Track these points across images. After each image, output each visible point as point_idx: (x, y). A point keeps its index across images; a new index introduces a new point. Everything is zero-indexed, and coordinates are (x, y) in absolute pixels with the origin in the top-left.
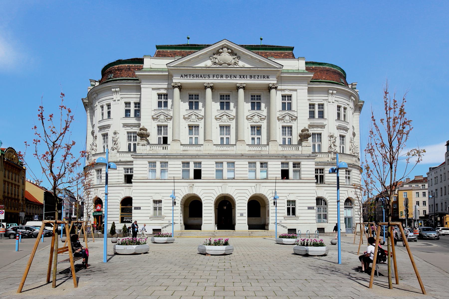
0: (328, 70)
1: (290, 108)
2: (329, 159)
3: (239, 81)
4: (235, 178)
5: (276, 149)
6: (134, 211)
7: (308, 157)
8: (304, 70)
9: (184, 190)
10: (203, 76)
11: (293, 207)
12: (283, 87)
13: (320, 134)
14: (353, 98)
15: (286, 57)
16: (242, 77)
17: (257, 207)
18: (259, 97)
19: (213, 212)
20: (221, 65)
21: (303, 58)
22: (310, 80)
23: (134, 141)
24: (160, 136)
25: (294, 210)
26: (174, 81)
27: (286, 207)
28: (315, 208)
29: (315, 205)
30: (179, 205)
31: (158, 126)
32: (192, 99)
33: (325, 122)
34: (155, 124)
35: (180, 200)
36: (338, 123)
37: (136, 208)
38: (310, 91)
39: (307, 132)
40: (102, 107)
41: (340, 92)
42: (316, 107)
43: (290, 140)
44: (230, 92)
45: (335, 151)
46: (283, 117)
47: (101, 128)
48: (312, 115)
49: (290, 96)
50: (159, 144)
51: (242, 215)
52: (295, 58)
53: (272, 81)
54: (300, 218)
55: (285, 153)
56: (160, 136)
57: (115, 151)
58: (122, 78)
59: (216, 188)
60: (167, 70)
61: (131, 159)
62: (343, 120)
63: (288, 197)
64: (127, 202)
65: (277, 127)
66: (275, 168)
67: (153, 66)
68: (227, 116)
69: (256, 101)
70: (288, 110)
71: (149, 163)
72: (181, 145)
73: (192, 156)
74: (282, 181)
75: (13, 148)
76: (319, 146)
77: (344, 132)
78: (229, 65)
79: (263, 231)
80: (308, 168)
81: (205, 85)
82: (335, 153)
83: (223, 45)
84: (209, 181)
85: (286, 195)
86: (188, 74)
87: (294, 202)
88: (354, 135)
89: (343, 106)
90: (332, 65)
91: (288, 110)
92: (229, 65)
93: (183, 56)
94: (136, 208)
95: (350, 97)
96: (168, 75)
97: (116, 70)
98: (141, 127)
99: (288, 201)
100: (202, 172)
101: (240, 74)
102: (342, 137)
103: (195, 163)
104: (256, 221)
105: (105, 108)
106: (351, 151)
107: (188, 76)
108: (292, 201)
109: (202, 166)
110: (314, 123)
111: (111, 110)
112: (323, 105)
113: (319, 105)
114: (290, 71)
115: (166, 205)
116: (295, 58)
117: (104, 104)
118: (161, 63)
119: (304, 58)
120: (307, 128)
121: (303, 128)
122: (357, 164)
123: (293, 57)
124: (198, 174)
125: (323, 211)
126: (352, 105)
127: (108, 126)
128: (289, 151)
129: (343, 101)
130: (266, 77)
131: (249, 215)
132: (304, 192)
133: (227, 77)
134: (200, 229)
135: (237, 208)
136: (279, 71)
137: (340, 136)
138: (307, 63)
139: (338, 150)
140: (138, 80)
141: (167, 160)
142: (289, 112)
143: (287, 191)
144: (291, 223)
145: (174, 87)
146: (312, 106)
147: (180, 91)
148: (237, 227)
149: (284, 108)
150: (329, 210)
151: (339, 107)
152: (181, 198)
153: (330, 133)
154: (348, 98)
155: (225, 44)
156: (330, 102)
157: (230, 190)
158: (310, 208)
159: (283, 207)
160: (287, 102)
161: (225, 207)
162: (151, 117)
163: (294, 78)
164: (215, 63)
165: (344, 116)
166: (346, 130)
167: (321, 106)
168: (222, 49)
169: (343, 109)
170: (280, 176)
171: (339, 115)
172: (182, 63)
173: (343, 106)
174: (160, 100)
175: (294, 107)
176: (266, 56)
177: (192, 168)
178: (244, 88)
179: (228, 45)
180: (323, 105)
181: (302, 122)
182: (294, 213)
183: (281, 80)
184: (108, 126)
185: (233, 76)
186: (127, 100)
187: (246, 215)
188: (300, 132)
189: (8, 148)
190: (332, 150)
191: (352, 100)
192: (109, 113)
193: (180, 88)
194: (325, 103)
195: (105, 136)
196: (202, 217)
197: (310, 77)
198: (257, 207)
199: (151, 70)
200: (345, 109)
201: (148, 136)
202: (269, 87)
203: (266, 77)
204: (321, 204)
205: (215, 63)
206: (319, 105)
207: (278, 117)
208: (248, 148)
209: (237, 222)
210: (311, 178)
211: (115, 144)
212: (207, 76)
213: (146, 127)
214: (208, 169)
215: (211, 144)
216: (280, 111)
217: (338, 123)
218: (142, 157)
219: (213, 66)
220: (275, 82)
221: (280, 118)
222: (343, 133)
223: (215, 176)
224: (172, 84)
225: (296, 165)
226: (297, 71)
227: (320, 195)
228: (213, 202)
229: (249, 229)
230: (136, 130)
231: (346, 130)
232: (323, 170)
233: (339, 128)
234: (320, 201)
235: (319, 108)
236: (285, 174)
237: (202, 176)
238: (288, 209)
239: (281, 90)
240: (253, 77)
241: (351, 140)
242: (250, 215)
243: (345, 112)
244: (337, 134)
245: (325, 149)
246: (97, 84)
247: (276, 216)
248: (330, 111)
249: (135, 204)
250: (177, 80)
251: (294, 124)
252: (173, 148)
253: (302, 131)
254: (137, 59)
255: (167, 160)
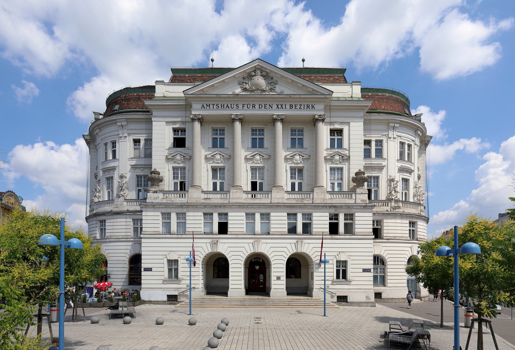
0: (388, 98)
1: (340, 146)
2: (388, 208)
3: (276, 112)
4: (271, 233)
5: (323, 197)
6: (143, 273)
7: (365, 208)
8: (359, 98)
9: (204, 249)
10: (230, 106)
11: (344, 268)
12: (333, 119)
13: (377, 178)
14: (419, 132)
15: (335, 82)
16: (280, 106)
17: (297, 266)
18: (301, 131)
19: (243, 270)
20: (253, 91)
21: (358, 82)
22: (367, 110)
23: (144, 186)
24: (176, 181)
25: (345, 272)
26: (194, 113)
27: (335, 268)
28: (372, 270)
29: (371, 267)
30: (201, 266)
31: (174, 168)
32: (256, 134)
33: (384, 163)
34: (171, 166)
35: (201, 260)
36: (400, 164)
37: (146, 270)
38: (367, 123)
39: (363, 175)
40: (106, 144)
41: (403, 124)
42: (373, 144)
43: (340, 185)
44: (264, 126)
45: (396, 199)
46: (332, 157)
47: (105, 170)
48: (367, 154)
49: (340, 132)
50: (175, 190)
51: (278, 278)
52: (347, 82)
53: (318, 111)
54: (353, 283)
55: (334, 201)
56: (176, 181)
57: (122, 199)
58: (128, 110)
59: (246, 246)
60: (184, 99)
61: (138, 208)
62: (406, 159)
63: (337, 257)
64: (135, 261)
65: (324, 169)
66: (321, 222)
67: (168, 95)
68: (260, 155)
69: (258, 137)
70: (338, 148)
71: (163, 214)
72: (203, 192)
73: (216, 206)
74: (330, 237)
75: (12, 192)
76: (376, 192)
77: (408, 175)
78: (264, 91)
79: (306, 298)
80: (364, 222)
81: (233, 116)
82: (397, 201)
83: (255, 67)
84: (238, 236)
85: (336, 254)
86: (211, 103)
87: (345, 262)
88: (419, 177)
89: (407, 142)
90: (393, 92)
91: (338, 148)
92: (264, 91)
93: (205, 81)
94: (146, 270)
95: (416, 132)
96: (186, 105)
97: (122, 100)
98: (153, 169)
99: (337, 261)
100: (229, 226)
101: (278, 103)
102: (406, 181)
103: (220, 214)
104: (296, 282)
105: (110, 146)
106: (416, 199)
107: (211, 106)
108: (343, 261)
109: (229, 218)
110: (372, 164)
111: (117, 149)
112: (381, 141)
113: (377, 141)
114: (340, 99)
115: (183, 269)
116: (347, 82)
117: (109, 141)
118: (178, 91)
119: (359, 82)
120: (362, 170)
121: (357, 171)
122: (423, 214)
123: (345, 81)
124: (223, 228)
125: (380, 272)
126: (417, 141)
127: (381, 168)
128: (338, 200)
129: (408, 137)
130: (311, 107)
131: (288, 276)
132: (357, 251)
133: (261, 107)
134: (225, 294)
135: (273, 270)
136: (327, 98)
137: (403, 179)
138: (363, 90)
139: (399, 196)
140: (148, 112)
141: (184, 211)
142: (340, 151)
143: (337, 248)
144: (341, 289)
145: (193, 120)
146: (367, 143)
147: (201, 125)
148: (271, 293)
149: (332, 146)
150: (389, 270)
151: (402, 144)
152: (203, 257)
153: (390, 176)
154: (414, 133)
155: (258, 65)
156: (391, 138)
157: (265, 247)
158: (365, 270)
159: (331, 269)
160: (218, 137)
161: (257, 270)
162: (164, 158)
163: (348, 107)
164: (245, 90)
165: (408, 154)
166: (410, 172)
167: (379, 143)
168: (255, 71)
169: (406, 146)
170: (328, 230)
171: (402, 154)
172: (202, 90)
173: (407, 142)
174: (332, 137)
175: (345, 145)
176: (311, 81)
177: (216, 220)
178: (282, 120)
179: (262, 67)
180: (381, 141)
181: (357, 163)
182: (345, 277)
183: (329, 108)
184: (113, 169)
185: (268, 106)
186: (136, 137)
187: (284, 278)
188: (353, 175)
189: (7, 192)
190: (393, 197)
191: (419, 135)
192: (114, 152)
193: (201, 120)
194: (385, 139)
195: (110, 179)
196: (228, 277)
197: (367, 106)
198: (297, 266)
199: (165, 98)
200: (409, 146)
201: (161, 181)
202: (314, 119)
203: (311, 107)
204: (378, 264)
205: (245, 90)
206: (377, 141)
207: (325, 157)
208: (286, 196)
209: (273, 287)
210: (367, 234)
211: (121, 190)
212: (235, 106)
213: (158, 170)
214: (237, 221)
215: (240, 191)
216: (327, 149)
217: (400, 164)
218: (154, 206)
219: (242, 93)
220: (322, 113)
221: (328, 157)
222: (406, 176)
223: (244, 230)
224: (191, 116)
225: (350, 217)
226: (350, 99)
227: (377, 253)
228: (243, 263)
229: (288, 294)
230: (146, 172)
231: (410, 172)
232: (380, 221)
233: (402, 170)
234: (379, 260)
235: (376, 145)
236: (334, 229)
237: (229, 230)
238: (338, 272)
239: (331, 123)
240: (294, 107)
241: (416, 184)
242: (289, 274)
243: (409, 150)
244: (398, 177)
245: (383, 195)
246: (101, 117)
247: (321, 278)
248: (391, 149)
249: (144, 264)
250: (197, 111)
251: (345, 167)
252: (194, 195)
253: (356, 174)
254: (148, 86)
255: (184, 211)
